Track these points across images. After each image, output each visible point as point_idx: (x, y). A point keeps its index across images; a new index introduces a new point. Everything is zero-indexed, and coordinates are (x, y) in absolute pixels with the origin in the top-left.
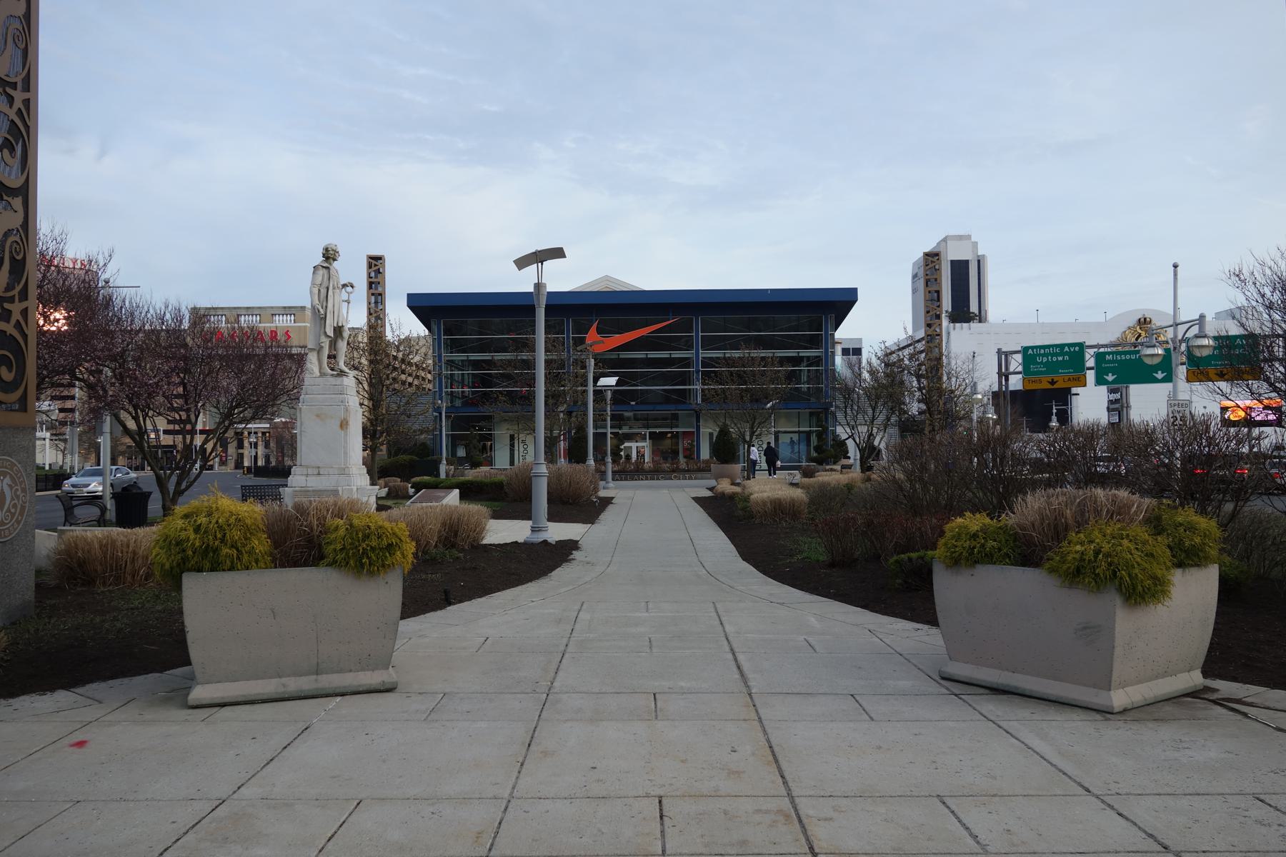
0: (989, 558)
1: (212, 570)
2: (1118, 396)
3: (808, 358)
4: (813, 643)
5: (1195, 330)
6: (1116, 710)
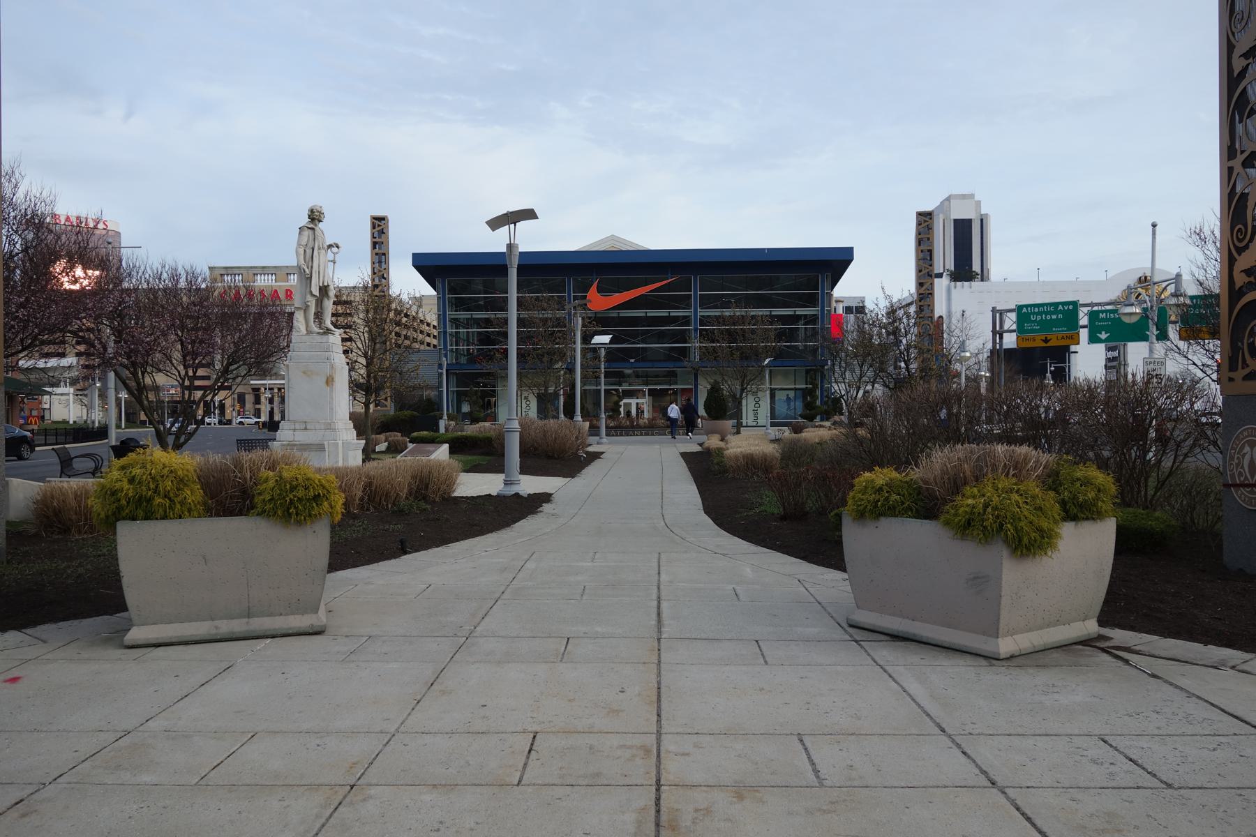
0: (891, 511)
1: (146, 518)
2: (1115, 354)
3: (806, 316)
4: (739, 592)
5: (1171, 289)
6: (1002, 657)
